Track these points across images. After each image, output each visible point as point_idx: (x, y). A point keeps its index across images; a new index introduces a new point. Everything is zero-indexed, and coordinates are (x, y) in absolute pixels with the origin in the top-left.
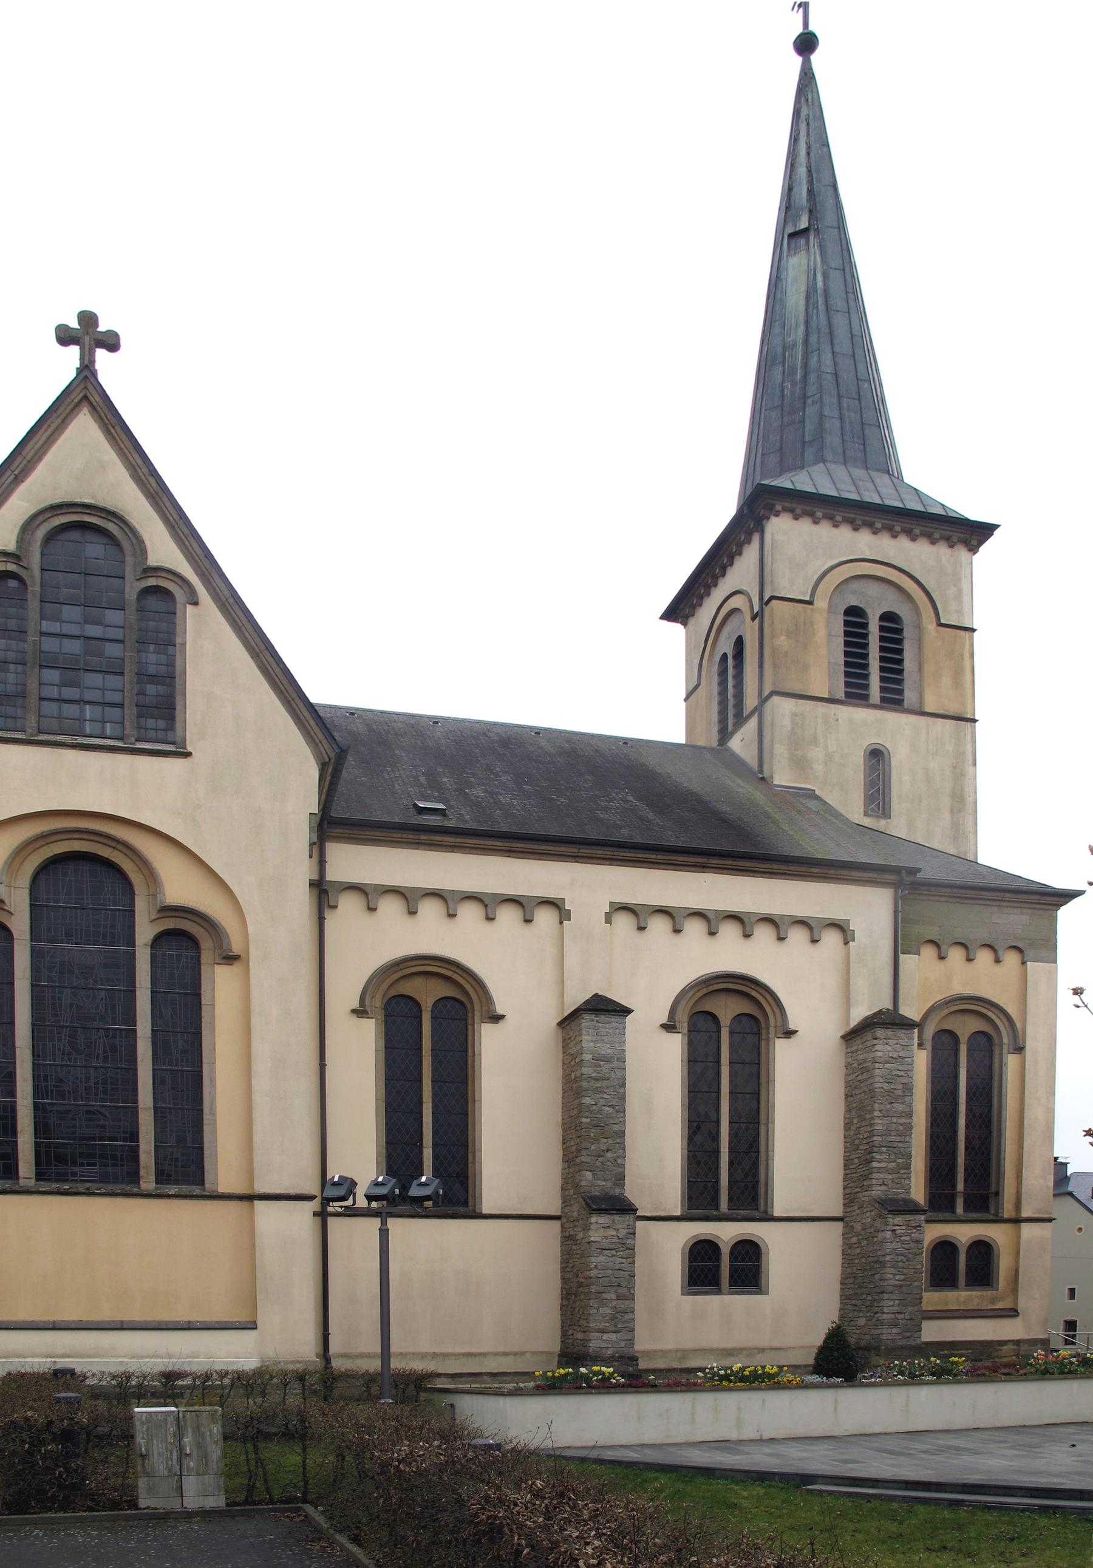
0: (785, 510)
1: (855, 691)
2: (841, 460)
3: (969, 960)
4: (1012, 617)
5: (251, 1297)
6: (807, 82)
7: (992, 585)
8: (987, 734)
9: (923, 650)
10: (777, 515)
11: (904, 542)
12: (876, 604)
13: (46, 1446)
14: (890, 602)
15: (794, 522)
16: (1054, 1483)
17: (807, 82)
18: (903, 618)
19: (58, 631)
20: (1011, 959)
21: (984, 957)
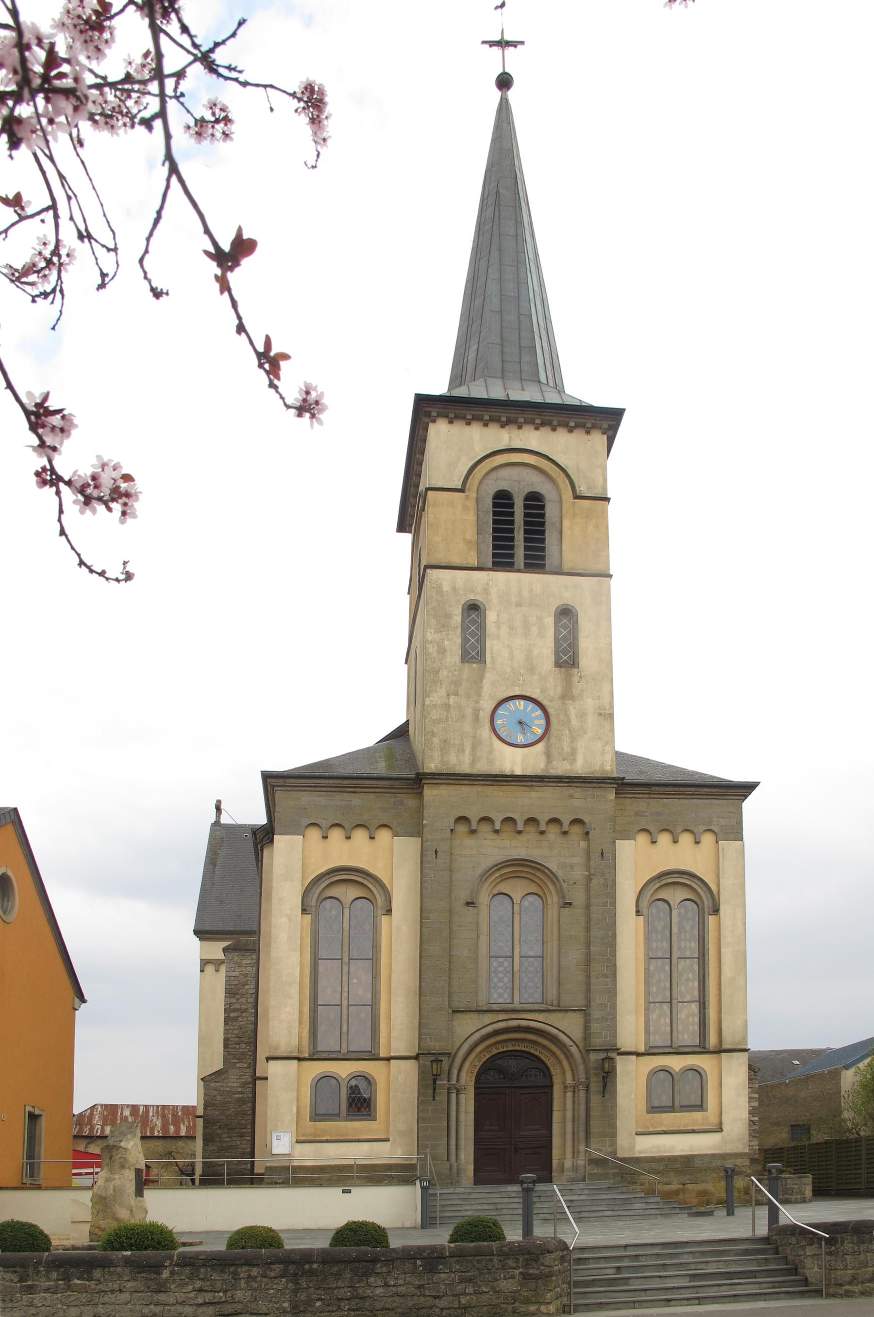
0: (439, 415)
1: (502, 559)
2: (500, 375)
3: (675, 842)
4: (638, 488)
5: (721, 1123)
6: (504, 112)
7: (627, 470)
8: (615, 584)
9: (568, 536)
10: (434, 421)
11: (545, 432)
12: (518, 484)
13: (21, 1243)
14: (535, 483)
15: (449, 425)
16: (40, 1145)
17: (504, 112)
18: (546, 496)
19: (695, 1007)
20: (708, 840)
21: (686, 839)
